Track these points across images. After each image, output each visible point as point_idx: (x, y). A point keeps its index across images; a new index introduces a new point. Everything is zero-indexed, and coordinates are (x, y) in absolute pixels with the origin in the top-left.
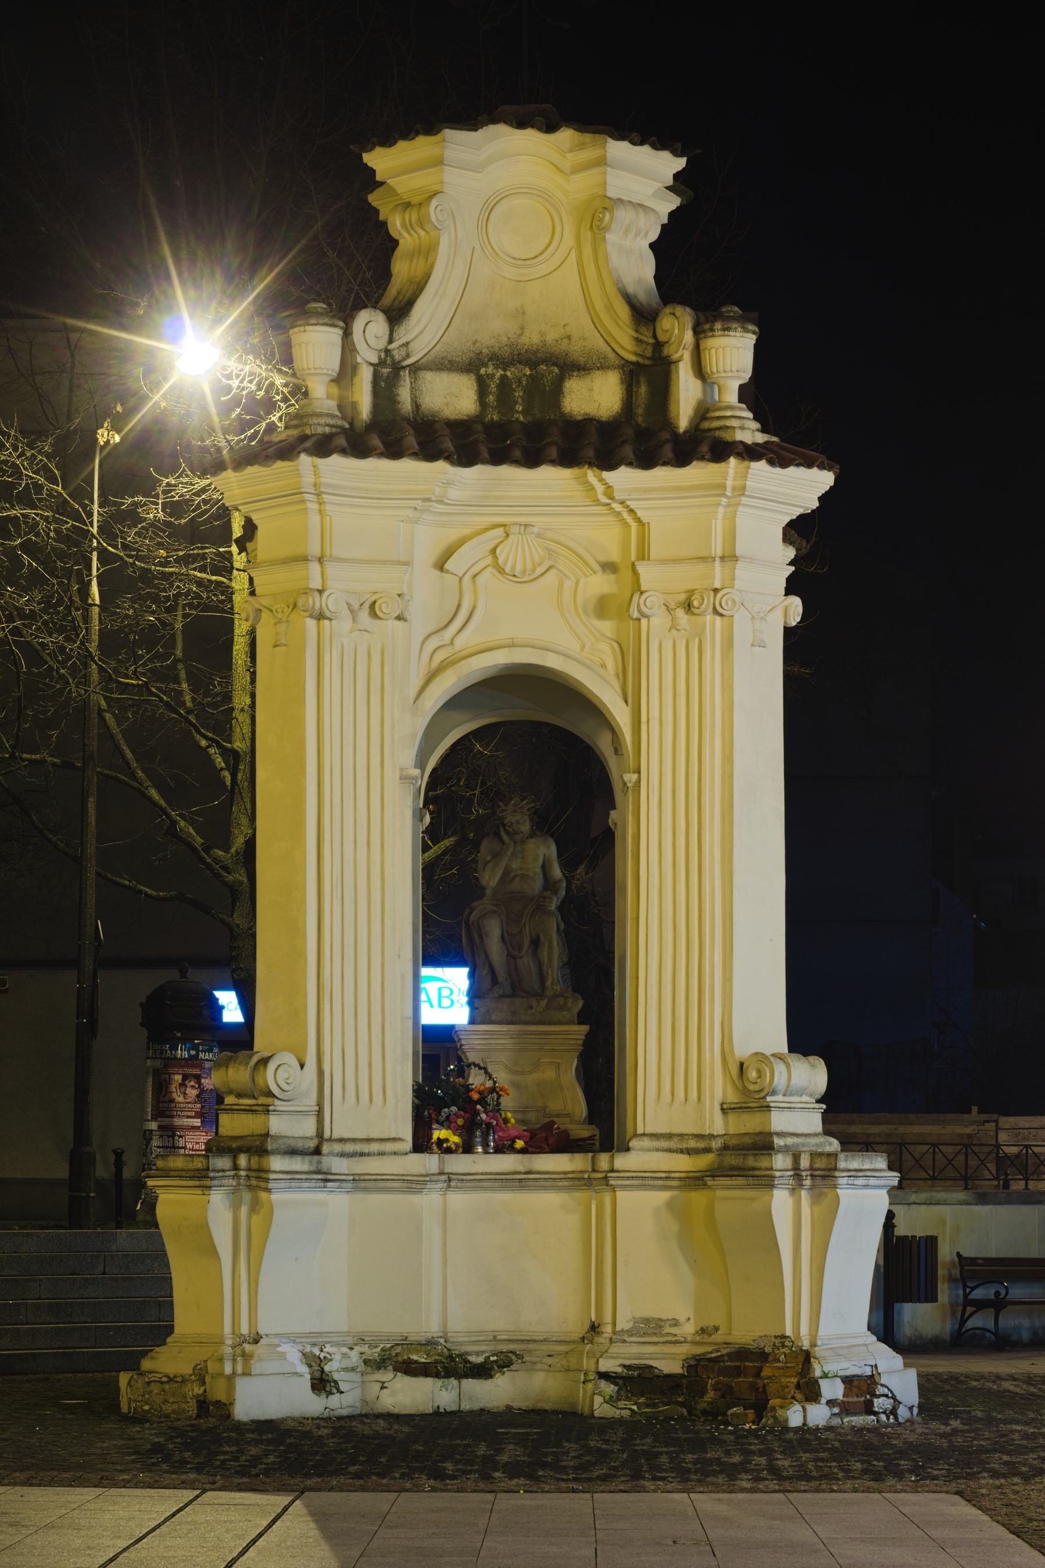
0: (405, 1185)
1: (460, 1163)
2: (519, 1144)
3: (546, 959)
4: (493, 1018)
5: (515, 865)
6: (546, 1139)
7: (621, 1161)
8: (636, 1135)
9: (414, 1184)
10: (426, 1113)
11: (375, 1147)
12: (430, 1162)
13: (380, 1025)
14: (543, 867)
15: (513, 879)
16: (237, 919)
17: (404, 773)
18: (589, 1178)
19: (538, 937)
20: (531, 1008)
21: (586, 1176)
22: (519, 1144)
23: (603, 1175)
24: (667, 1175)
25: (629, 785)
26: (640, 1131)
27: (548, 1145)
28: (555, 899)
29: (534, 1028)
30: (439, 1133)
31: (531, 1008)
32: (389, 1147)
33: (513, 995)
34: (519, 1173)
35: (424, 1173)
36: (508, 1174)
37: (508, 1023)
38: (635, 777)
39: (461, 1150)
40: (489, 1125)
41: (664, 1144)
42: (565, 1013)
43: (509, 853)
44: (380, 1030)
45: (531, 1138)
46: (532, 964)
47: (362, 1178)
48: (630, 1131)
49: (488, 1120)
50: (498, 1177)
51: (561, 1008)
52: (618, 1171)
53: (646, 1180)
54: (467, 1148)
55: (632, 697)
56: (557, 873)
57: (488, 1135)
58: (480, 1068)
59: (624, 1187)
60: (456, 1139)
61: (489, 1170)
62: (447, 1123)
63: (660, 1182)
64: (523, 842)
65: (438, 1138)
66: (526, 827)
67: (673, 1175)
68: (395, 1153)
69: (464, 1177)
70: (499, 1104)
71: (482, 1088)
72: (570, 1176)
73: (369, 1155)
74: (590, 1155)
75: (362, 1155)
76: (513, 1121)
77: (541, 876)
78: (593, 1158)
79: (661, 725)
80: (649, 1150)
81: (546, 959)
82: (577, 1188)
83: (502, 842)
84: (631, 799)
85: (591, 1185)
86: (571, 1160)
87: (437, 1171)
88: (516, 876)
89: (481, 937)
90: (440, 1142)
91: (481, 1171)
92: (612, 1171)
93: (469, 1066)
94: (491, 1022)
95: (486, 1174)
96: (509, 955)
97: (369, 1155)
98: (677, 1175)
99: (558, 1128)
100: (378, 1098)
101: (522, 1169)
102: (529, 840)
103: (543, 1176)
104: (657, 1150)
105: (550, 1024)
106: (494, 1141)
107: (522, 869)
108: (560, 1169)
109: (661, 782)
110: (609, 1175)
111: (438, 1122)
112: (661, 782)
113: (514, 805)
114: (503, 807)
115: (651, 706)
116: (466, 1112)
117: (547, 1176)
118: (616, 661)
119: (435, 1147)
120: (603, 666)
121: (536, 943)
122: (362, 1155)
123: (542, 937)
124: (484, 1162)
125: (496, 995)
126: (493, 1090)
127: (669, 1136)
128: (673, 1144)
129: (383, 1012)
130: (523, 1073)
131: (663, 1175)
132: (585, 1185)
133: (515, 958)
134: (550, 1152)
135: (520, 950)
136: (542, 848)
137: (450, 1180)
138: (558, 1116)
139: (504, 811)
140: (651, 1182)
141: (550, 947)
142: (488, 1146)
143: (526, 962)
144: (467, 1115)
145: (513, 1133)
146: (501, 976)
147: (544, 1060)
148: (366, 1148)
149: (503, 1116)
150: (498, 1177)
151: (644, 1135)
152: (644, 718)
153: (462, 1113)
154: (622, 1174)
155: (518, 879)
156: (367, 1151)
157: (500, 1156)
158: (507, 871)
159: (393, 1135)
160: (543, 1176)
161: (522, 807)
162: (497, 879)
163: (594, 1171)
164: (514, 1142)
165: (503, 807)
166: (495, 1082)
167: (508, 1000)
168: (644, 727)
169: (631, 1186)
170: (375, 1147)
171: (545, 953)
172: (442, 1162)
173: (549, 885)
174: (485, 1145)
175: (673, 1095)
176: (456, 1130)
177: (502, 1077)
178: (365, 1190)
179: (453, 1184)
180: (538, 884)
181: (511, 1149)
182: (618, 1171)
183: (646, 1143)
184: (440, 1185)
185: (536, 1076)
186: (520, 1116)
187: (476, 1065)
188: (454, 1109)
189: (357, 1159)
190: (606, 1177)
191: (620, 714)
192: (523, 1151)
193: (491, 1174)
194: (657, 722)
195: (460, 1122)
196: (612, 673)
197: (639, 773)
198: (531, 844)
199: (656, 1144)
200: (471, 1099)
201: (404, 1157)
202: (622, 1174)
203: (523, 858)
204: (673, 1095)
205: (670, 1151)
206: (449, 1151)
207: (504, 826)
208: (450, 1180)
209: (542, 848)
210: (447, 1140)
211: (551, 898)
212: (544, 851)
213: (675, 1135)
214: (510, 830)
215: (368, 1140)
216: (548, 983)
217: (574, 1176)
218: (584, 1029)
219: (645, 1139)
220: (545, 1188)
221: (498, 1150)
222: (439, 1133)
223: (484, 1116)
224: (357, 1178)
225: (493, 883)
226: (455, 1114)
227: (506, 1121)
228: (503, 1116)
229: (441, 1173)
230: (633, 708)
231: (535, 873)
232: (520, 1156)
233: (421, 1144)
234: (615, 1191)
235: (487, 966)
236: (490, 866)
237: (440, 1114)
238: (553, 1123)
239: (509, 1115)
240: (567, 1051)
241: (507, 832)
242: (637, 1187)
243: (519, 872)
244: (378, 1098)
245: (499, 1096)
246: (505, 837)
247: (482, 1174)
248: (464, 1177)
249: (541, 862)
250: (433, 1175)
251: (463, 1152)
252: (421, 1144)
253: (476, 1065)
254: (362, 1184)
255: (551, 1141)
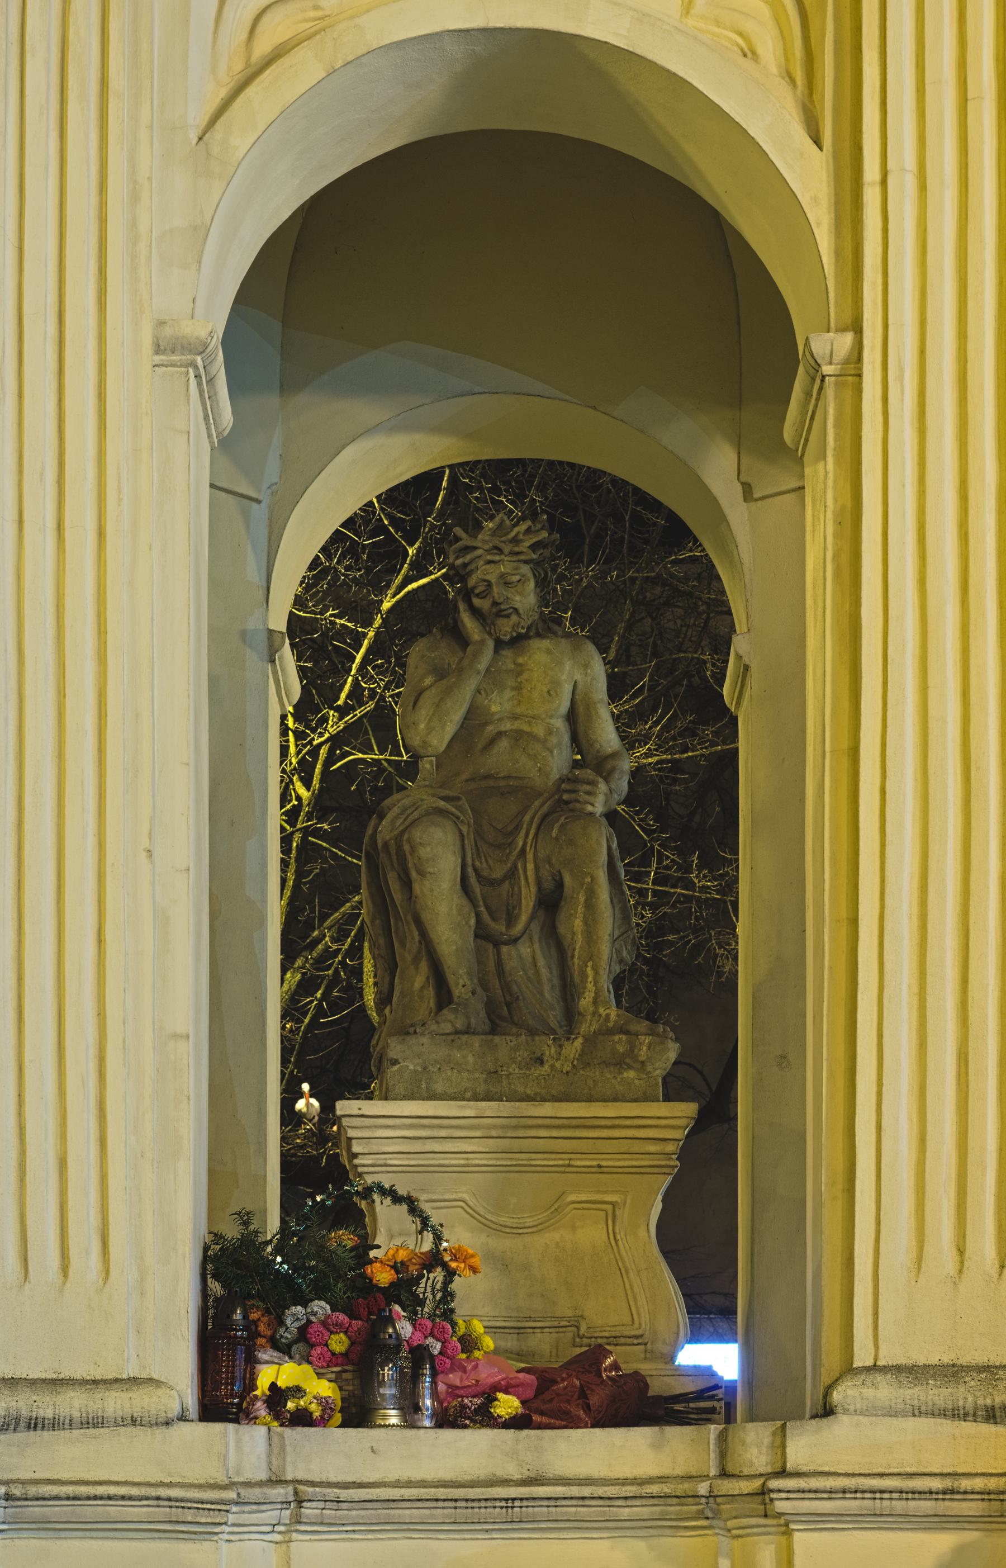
0: (162, 1512)
1: (332, 1454)
2: (507, 1405)
3: (580, 939)
4: (439, 1087)
5: (498, 704)
6: (583, 1394)
7: (807, 1446)
8: (848, 1370)
9: (188, 1511)
10: (238, 1315)
11: (72, 1403)
12: (246, 1447)
13: (93, 1052)
14: (571, 717)
15: (492, 741)
16: (215, 1287)
17: (168, 331)
18: (711, 1496)
19: (560, 885)
20: (541, 1061)
21: (703, 1489)
22: (507, 1405)
23: (756, 1484)
24: (948, 1483)
25: (827, 369)
26: (862, 1358)
27: (587, 1408)
28: (603, 787)
29: (547, 1109)
30: (274, 1372)
31: (541, 1061)
32: (114, 1403)
33: (493, 1031)
34: (505, 1482)
35: (221, 1478)
36: (472, 1485)
37: (476, 1098)
38: (847, 339)
39: (338, 1418)
40: (419, 1355)
41: (938, 1394)
42: (631, 1074)
43: (482, 665)
44: (92, 1066)
45: (540, 1391)
46: (541, 962)
47: (33, 1490)
48: (831, 1361)
49: (418, 1339)
50: (442, 1493)
51: (620, 1063)
52: (798, 1475)
53: (881, 1501)
54: (358, 1413)
55: (837, 120)
56: (607, 736)
57: (416, 1377)
58: (397, 1199)
59: (818, 1521)
60: (325, 1388)
61: (417, 1475)
62: (302, 1345)
63: (927, 1506)
64: (518, 641)
65: (273, 1386)
66: (526, 599)
67: (965, 1484)
68: (134, 1422)
69: (344, 1494)
70: (448, 1296)
71: (402, 1255)
72: (654, 1489)
73: (55, 1424)
74: (713, 1430)
75: (34, 1424)
76: (489, 1343)
77: (566, 738)
78: (722, 1438)
79: (922, 187)
80: (892, 1413)
81: (580, 939)
82: (676, 1526)
83: (462, 641)
84: (831, 411)
85: (717, 1514)
86: (657, 1446)
87: (263, 1475)
88: (500, 734)
89: (407, 884)
90: (277, 1396)
91: (392, 1477)
92: (782, 1473)
93: (367, 1193)
94: (432, 1096)
95: (409, 1484)
96: (481, 934)
97: (55, 1424)
98: (978, 1483)
99: (615, 1366)
100: (86, 1261)
101: (513, 1471)
102: (536, 644)
103: (575, 1491)
104: (917, 1412)
105: (590, 1099)
106: (435, 1395)
107: (515, 717)
108: (626, 1471)
109: (922, 352)
110: (773, 1484)
111: (275, 1344)
112: (922, 352)
113: (494, 533)
114: (466, 540)
115: (895, 136)
116: (352, 1316)
117: (587, 1491)
118: (784, 36)
119: (261, 1409)
120: (750, 53)
121: (551, 902)
122: (34, 1424)
123: (567, 879)
124: (404, 1451)
125: (447, 1028)
126: (434, 1260)
127: (952, 1372)
128: (966, 1394)
129: (101, 1014)
130: (517, 1231)
131: (936, 1484)
132: (700, 1515)
133: (497, 944)
134: (594, 1426)
135: (511, 920)
136: (568, 665)
137: (300, 1503)
138: (615, 1340)
139: (468, 549)
140: (899, 1506)
141: (590, 906)
142: (417, 1409)
143: (527, 956)
144: (357, 1324)
145: (487, 1375)
146: (461, 981)
147: (572, 1197)
148: (46, 1405)
149: (462, 1329)
150: (442, 1493)
151: (874, 1368)
152: (871, 172)
153: (342, 1317)
154: (814, 1483)
155: (504, 744)
156: (49, 1414)
157: (448, 1434)
158: (474, 721)
159: (131, 1370)
160: (575, 1491)
161: (515, 541)
162: (450, 730)
163: (724, 1474)
164: (491, 1399)
165: (466, 540)
166: (438, 1238)
167: (476, 1041)
168: (871, 197)
169: (839, 1516)
170: (72, 1403)
171: (578, 923)
172: (275, 1449)
173: (588, 761)
174: (410, 1410)
175: (961, 1252)
176: (326, 1364)
177: (459, 1236)
178: (44, 1526)
179: (309, 1511)
180: (559, 759)
181: (484, 1417)
182: (798, 1475)
183: (884, 1391)
184: (270, 1515)
185: (552, 1237)
186: (510, 1342)
187: (384, 1192)
188: (320, 1307)
189: (22, 1436)
190: (763, 1492)
191: (806, 174)
192: (517, 1423)
193: (423, 1484)
194: (910, 182)
195: (338, 1343)
196: (775, 70)
197: (857, 328)
198: (540, 653)
199: (913, 1394)
200: (368, 1286)
201: (160, 1432)
202: (814, 1483)
203: (518, 688)
204: (961, 1252)
205: (957, 1414)
206: (302, 1419)
207: (467, 594)
208: (300, 1502)
209: (568, 665)
210: (297, 1391)
211: (592, 783)
212: (570, 673)
213: (968, 1368)
214: (482, 604)
215: (55, 1384)
216: (585, 1002)
217: (666, 1489)
218: (686, 1110)
219: (879, 1378)
220: (580, 1525)
221: (447, 1419)
222: (274, 1372)
223: (405, 1328)
224: (17, 1491)
225: (440, 740)
226: (324, 1323)
227: (469, 1343)
228: (462, 1329)
229: (276, 1481)
230: (836, 155)
231: (550, 732)
232: (510, 1434)
233: (222, 1396)
234: (788, 1533)
235: (424, 966)
236: (427, 702)
237: (281, 1323)
238: (598, 1352)
239: (478, 1327)
240: (638, 1171)
241: (476, 613)
242: (857, 1520)
243: (507, 726)
244: (86, 1261)
245: (450, 1274)
246: (469, 623)
247: (397, 1484)
248: (344, 1494)
249: (564, 705)
250: (248, 1484)
251: (344, 1425)
252: (222, 1396)
253: (384, 1192)
254: (36, 1510)
255: (594, 1400)
